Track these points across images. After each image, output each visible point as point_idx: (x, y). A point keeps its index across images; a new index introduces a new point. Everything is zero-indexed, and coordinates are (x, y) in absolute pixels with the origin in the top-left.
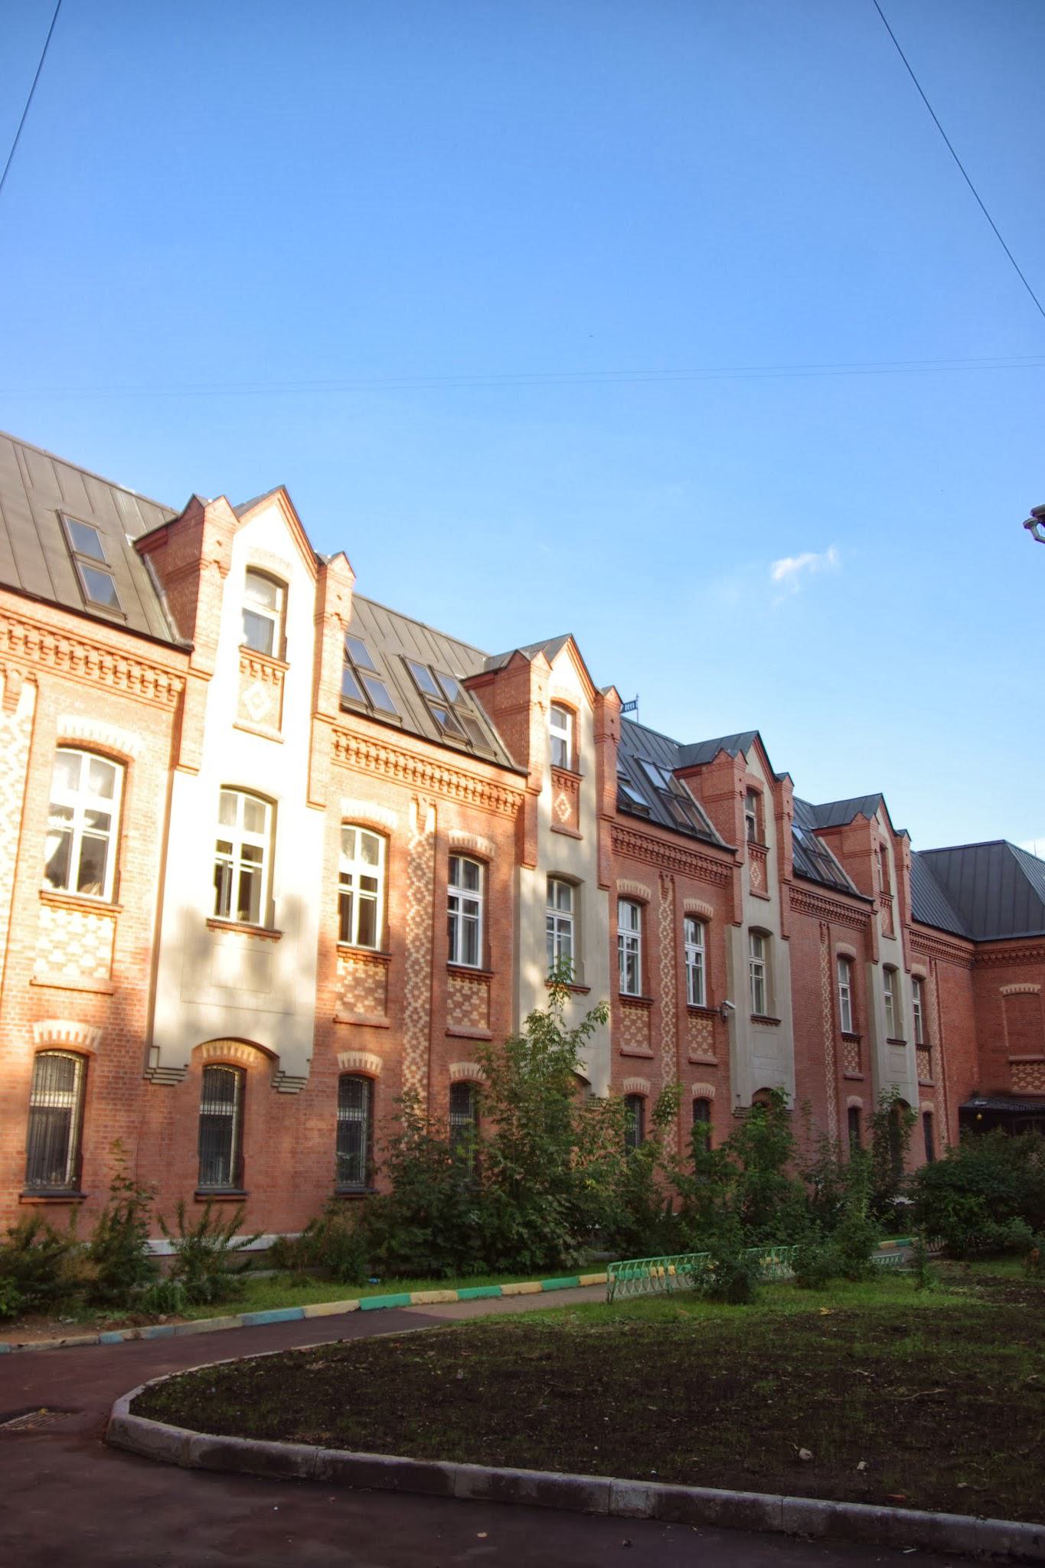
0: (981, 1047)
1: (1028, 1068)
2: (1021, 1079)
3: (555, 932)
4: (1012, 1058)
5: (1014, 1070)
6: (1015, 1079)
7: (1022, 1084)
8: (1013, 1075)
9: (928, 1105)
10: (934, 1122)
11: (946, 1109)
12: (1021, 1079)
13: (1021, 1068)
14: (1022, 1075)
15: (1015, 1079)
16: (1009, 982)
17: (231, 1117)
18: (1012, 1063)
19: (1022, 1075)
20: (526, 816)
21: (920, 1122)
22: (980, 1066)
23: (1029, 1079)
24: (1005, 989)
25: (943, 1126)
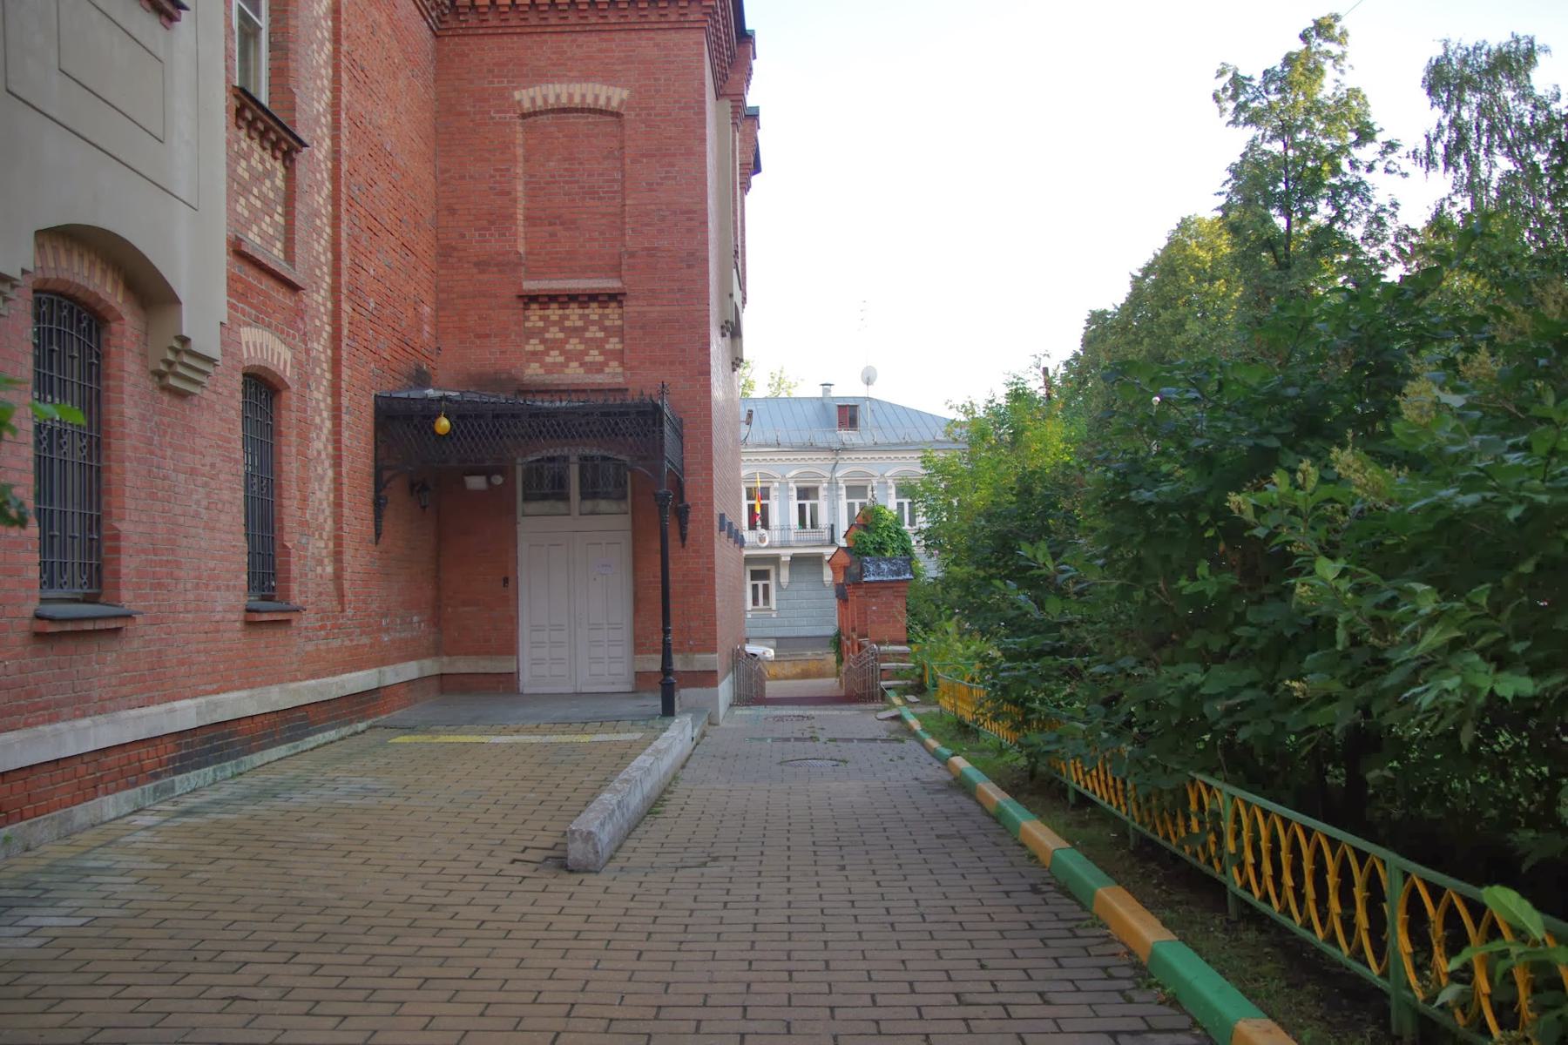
0: (445, 252)
1: (574, 314)
2: (551, 345)
3: (56, 508)
4: (530, 286)
5: (535, 317)
6: (534, 345)
7: (555, 357)
8: (531, 333)
9: (263, 345)
10: (289, 418)
11: (336, 391)
12: (551, 345)
13: (554, 313)
14: (554, 333)
15: (534, 345)
16: (541, 77)
17: (526, 499)
18: (530, 299)
19: (554, 333)
20: (762, 708)
21: (223, 405)
22: (440, 307)
23: (574, 344)
24: (527, 96)
25: (320, 444)
